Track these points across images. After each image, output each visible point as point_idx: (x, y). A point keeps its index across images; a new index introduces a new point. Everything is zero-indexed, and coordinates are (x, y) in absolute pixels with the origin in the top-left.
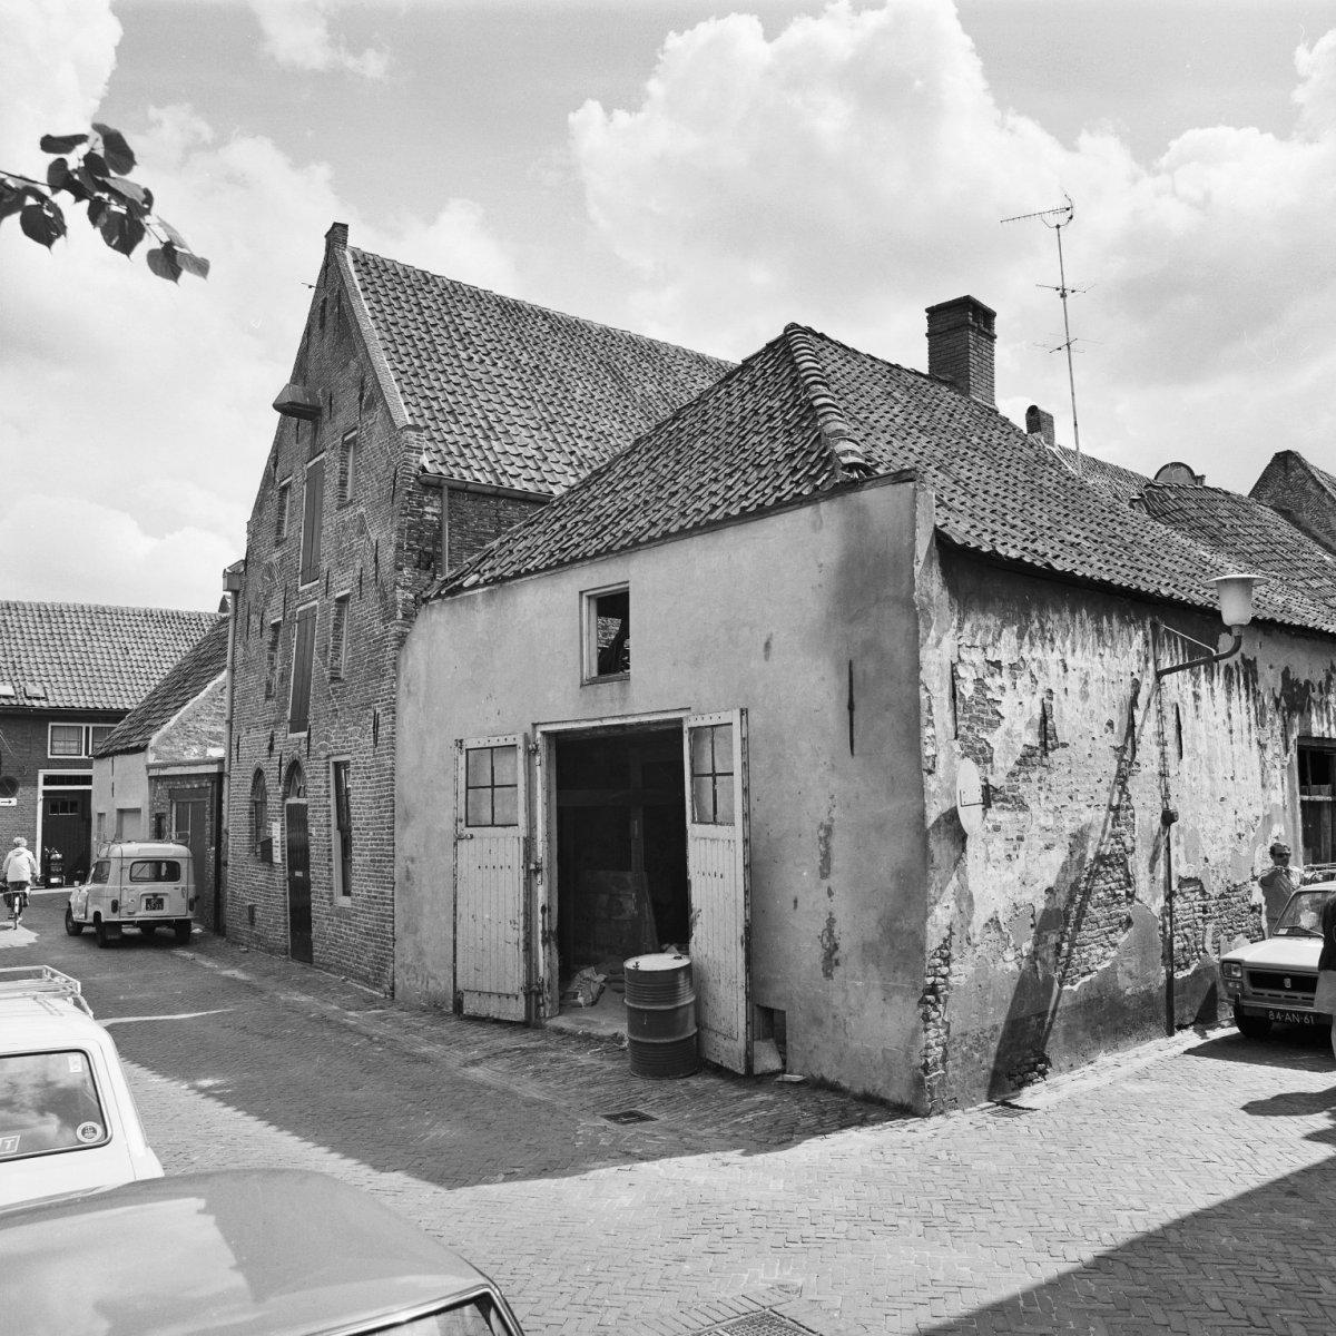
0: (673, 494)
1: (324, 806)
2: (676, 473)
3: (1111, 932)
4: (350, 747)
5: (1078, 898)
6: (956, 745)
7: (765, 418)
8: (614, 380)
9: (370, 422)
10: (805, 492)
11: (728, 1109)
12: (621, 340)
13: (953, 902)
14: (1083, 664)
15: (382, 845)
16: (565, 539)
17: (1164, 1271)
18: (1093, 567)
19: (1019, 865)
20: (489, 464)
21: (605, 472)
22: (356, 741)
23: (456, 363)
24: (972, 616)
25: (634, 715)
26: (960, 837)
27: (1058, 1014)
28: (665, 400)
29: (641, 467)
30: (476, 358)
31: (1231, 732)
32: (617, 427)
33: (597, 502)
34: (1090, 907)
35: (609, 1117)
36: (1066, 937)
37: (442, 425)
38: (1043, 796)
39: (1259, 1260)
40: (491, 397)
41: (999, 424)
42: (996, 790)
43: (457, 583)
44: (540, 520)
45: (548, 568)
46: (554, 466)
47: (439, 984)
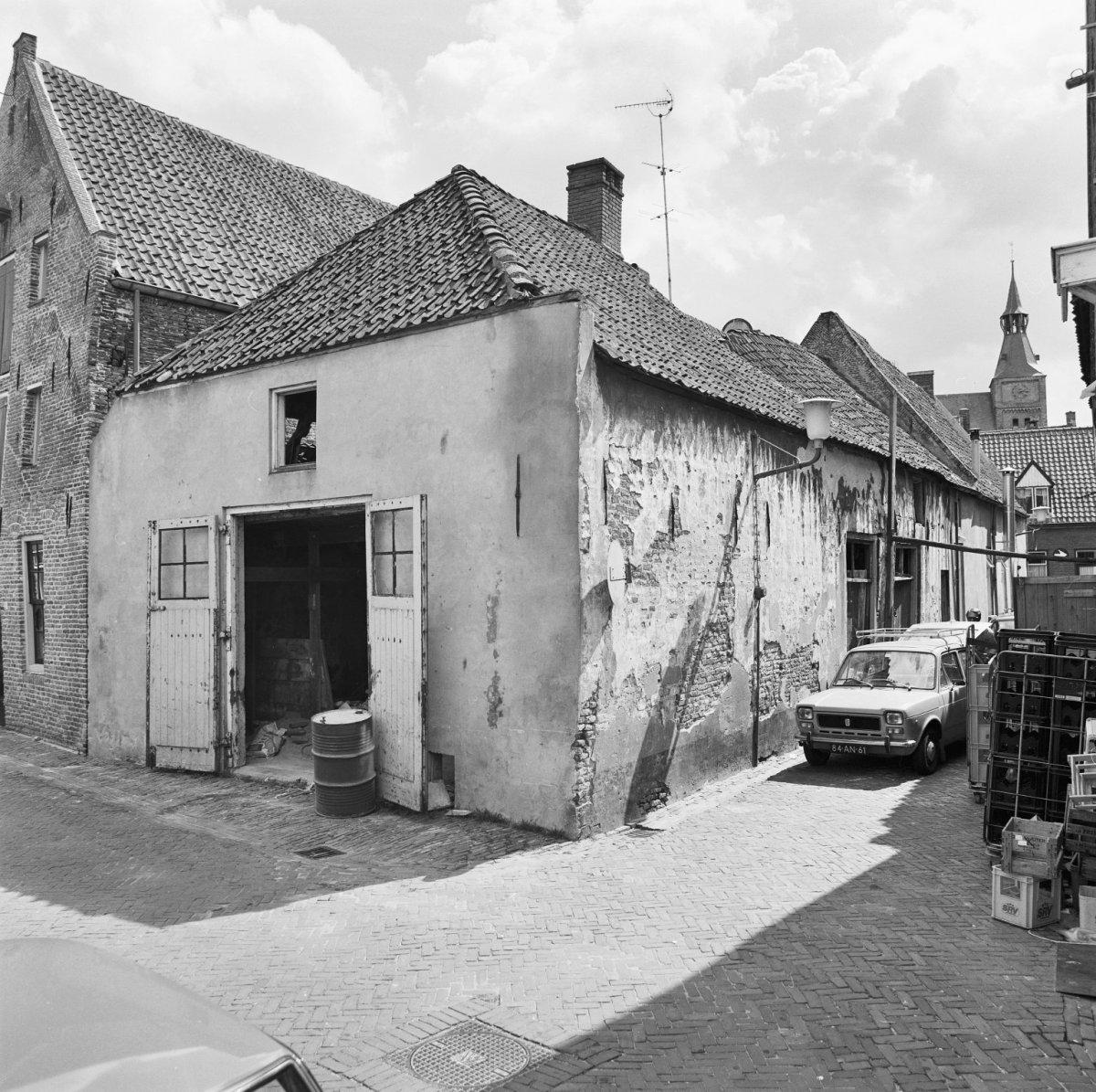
0: (357, 306)
1: (16, 582)
2: (358, 288)
3: (716, 685)
4: (43, 527)
5: (693, 659)
6: (606, 529)
7: (439, 243)
8: (291, 210)
9: (62, 226)
10: (481, 307)
11: (409, 842)
12: (296, 175)
13: (600, 661)
14: (702, 467)
15: (75, 617)
16: (255, 342)
17: (794, 957)
18: (710, 388)
19: (651, 630)
20: (179, 273)
21: (291, 285)
22: (49, 522)
23: (145, 180)
24: (620, 420)
25: (319, 501)
26: (608, 606)
27: (676, 752)
28: (335, 231)
29: (325, 282)
30: (164, 177)
31: (803, 526)
32: (294, 250)
33: (284, 310)
34: (701, 665)
35: (301, 853)
36: (684, 690)
37: (132, 234)
38: (669, 574)
39: (864, 943)
40: (179, 213)
41: (625, 269)
42: (635, 568)
43: (151, 378)
44: (230, 325)
45: (240, 367)
46: (238, 281)
47: (132, 741)
